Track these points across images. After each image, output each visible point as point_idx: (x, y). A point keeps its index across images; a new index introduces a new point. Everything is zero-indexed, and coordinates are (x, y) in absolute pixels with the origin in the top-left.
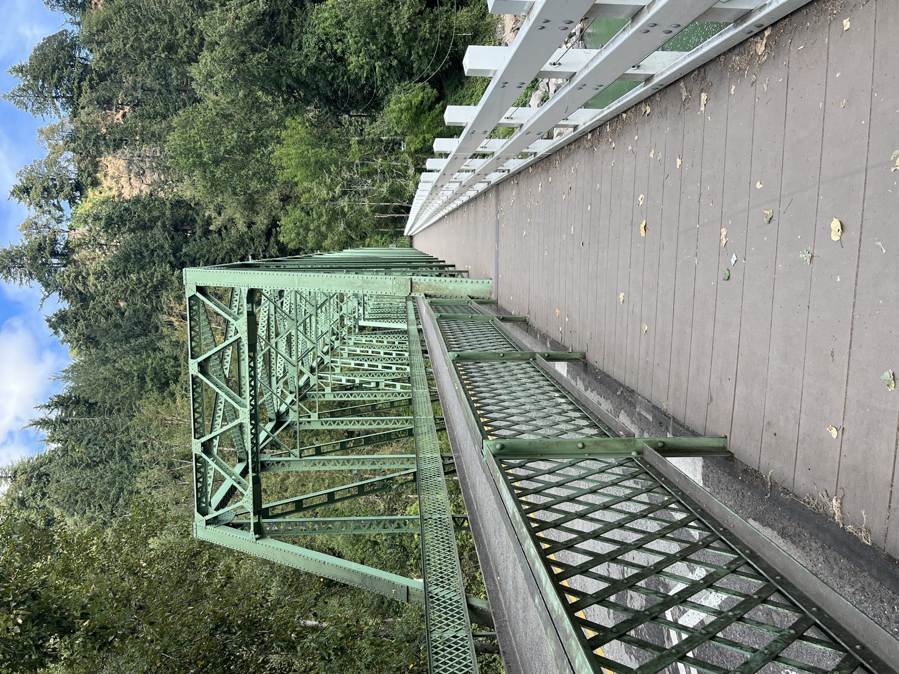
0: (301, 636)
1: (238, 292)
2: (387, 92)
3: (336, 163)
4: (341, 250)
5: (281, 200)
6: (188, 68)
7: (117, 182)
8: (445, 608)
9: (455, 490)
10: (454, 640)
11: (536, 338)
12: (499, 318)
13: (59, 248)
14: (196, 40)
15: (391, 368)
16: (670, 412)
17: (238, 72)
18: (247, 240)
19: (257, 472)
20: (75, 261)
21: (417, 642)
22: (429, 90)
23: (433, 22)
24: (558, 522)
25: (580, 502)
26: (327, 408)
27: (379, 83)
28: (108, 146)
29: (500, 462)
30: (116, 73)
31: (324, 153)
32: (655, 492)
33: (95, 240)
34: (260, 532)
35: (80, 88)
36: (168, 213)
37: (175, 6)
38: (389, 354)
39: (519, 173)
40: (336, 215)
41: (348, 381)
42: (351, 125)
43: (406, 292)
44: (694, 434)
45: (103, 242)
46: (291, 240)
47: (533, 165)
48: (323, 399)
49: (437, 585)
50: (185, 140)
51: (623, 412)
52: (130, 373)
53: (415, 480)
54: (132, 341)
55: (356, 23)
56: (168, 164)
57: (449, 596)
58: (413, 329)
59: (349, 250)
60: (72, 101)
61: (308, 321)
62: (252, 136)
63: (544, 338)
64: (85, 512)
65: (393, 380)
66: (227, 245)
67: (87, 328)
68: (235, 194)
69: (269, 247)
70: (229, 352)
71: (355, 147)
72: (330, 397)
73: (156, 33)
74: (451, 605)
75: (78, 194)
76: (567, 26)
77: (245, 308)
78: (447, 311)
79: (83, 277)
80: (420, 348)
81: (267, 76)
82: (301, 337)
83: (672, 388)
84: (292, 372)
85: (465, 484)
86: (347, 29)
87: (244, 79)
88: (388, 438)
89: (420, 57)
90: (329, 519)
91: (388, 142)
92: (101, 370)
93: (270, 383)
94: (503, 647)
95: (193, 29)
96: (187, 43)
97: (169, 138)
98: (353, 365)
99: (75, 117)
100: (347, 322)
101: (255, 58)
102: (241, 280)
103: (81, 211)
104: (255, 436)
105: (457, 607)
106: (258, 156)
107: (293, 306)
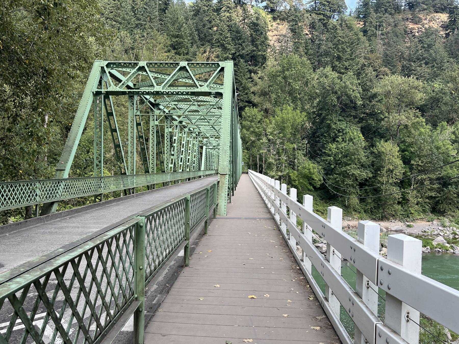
0: (40, 114)
1: (221, 87)
2: (318, 162)
3: (284, 136)
4: (241, 138)
5: (266, 109)
6: (329, 66)
7: (275, 29)
8: (53, 190)
9: (116, 195)
10: (35, 195)
11: (196, 239)
12: (207, 220)
14: (342, 71)
15: (181, 162)
16: (157, 313)
17: (328, 90)
18: (246, 91)
19: (128, 94)
20: (236, 7)
21: (34, 174)
22: (319, 183)
23: (352, 185)
24: (101, 259)
25: (111, 269)
26: (161, 128)
27: (323, 158)
28: (292, 26)
29: (133, 226)
30: (327, 32)
31: (289, 131)
32: (116, 308)
33: (247, 17)
34: (97, 94)
35: (320, 14)
36: (260, 53)
37: (359, 62)
38: (188, 160)
39: (280, 230)
40: (258, 136)
41: (175, 140)
42: (302, 144)
43: (221, 172)
44: (146, 327)
45: (246, 21)
46: (246, 113)
47: (284, 238)
48: (166, 127)
49: (66, 185)
50: (296, 63)
51: (157, 286)
52: (181, 31)
53: (122, 174)
54: (197, 32)
55: (351, 148)
56: (284, 54)
57: (59, 192)
58: (201, 173)
59: (241, 142)
60: (313, 10)
61: (206, 121)
62: (297, 96)
63: (196, 244)
64: (109, 4)
65: (175, 163)
66: (244, 81)
67: (203, 11)
68: (269, 86)
69: (242, 104)
70: (191, 82)
71: (291, 146)
72: (166, 131)
73: (346, 52)
74: (54, 193)
75: (269, 10)
76: (353, 260)
77: (213, 91)
78: (210, 193)
79: (229, 10)
80: (191, 177)
81: (326, 104)
82: (198, 117)
83: (170, 314)
84: (180, 113)
85: (119, 200)
86: (349, 143)
87: (324, 93)
88: (145, 160)
89: (335, 179)
90: (103, 130)
91: (294, 162)
92: (182, 17)
93: (175, 101)
94: (30, 221)
95: (348, 69)
96: (341, 66)
97: (296, 56)
98: (183, 142)
99: (306, 11)
100: (205, 140)
101: (334, 98)
102: (227, 89)
103: (261, 11)
104: (148, 93)
105: (53, 196)
106: (287, 99)
107: (213, 114)
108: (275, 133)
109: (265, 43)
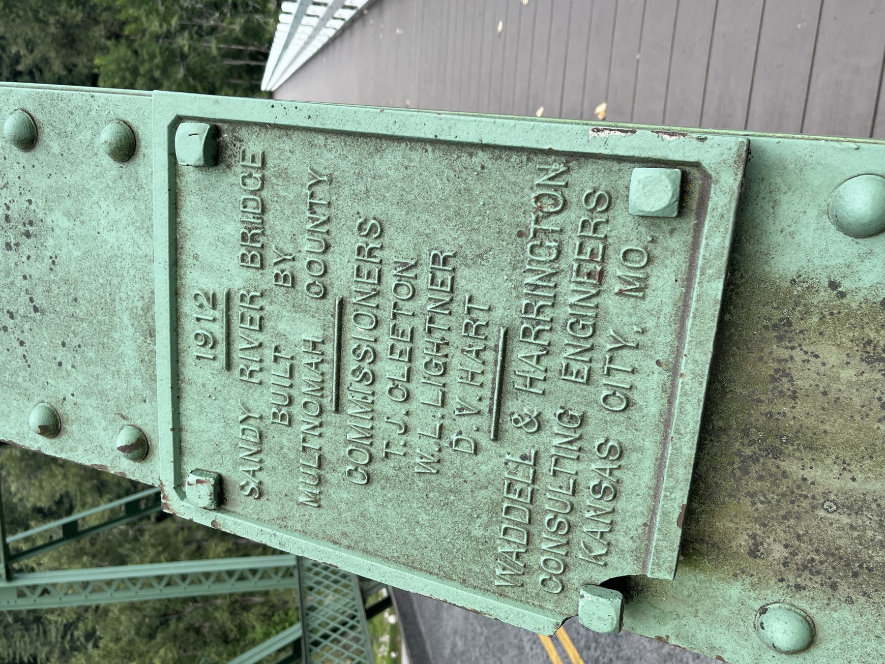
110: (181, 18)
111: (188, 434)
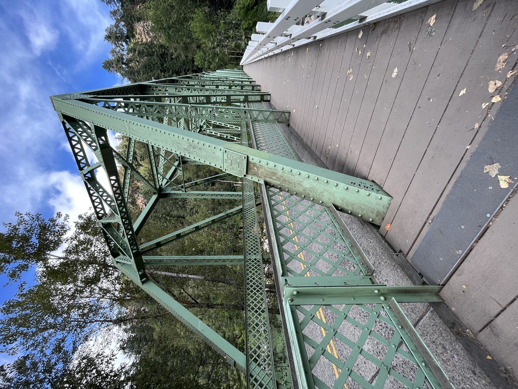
7: (141, 36)
13: (125, 61)
40: (215, 55)
50: (156, 16)
71: (222, 25)
108: (212, 39)
109: (150, 45)
110: (217, 42)
111: (505, 360)
